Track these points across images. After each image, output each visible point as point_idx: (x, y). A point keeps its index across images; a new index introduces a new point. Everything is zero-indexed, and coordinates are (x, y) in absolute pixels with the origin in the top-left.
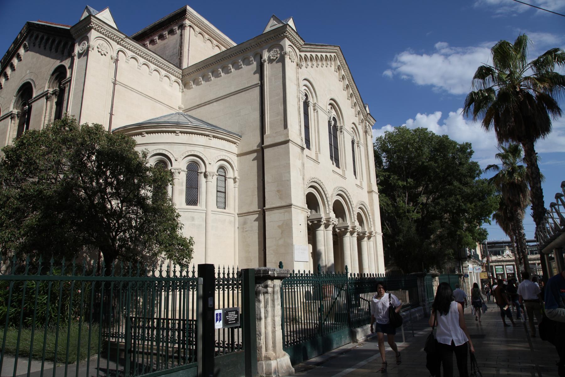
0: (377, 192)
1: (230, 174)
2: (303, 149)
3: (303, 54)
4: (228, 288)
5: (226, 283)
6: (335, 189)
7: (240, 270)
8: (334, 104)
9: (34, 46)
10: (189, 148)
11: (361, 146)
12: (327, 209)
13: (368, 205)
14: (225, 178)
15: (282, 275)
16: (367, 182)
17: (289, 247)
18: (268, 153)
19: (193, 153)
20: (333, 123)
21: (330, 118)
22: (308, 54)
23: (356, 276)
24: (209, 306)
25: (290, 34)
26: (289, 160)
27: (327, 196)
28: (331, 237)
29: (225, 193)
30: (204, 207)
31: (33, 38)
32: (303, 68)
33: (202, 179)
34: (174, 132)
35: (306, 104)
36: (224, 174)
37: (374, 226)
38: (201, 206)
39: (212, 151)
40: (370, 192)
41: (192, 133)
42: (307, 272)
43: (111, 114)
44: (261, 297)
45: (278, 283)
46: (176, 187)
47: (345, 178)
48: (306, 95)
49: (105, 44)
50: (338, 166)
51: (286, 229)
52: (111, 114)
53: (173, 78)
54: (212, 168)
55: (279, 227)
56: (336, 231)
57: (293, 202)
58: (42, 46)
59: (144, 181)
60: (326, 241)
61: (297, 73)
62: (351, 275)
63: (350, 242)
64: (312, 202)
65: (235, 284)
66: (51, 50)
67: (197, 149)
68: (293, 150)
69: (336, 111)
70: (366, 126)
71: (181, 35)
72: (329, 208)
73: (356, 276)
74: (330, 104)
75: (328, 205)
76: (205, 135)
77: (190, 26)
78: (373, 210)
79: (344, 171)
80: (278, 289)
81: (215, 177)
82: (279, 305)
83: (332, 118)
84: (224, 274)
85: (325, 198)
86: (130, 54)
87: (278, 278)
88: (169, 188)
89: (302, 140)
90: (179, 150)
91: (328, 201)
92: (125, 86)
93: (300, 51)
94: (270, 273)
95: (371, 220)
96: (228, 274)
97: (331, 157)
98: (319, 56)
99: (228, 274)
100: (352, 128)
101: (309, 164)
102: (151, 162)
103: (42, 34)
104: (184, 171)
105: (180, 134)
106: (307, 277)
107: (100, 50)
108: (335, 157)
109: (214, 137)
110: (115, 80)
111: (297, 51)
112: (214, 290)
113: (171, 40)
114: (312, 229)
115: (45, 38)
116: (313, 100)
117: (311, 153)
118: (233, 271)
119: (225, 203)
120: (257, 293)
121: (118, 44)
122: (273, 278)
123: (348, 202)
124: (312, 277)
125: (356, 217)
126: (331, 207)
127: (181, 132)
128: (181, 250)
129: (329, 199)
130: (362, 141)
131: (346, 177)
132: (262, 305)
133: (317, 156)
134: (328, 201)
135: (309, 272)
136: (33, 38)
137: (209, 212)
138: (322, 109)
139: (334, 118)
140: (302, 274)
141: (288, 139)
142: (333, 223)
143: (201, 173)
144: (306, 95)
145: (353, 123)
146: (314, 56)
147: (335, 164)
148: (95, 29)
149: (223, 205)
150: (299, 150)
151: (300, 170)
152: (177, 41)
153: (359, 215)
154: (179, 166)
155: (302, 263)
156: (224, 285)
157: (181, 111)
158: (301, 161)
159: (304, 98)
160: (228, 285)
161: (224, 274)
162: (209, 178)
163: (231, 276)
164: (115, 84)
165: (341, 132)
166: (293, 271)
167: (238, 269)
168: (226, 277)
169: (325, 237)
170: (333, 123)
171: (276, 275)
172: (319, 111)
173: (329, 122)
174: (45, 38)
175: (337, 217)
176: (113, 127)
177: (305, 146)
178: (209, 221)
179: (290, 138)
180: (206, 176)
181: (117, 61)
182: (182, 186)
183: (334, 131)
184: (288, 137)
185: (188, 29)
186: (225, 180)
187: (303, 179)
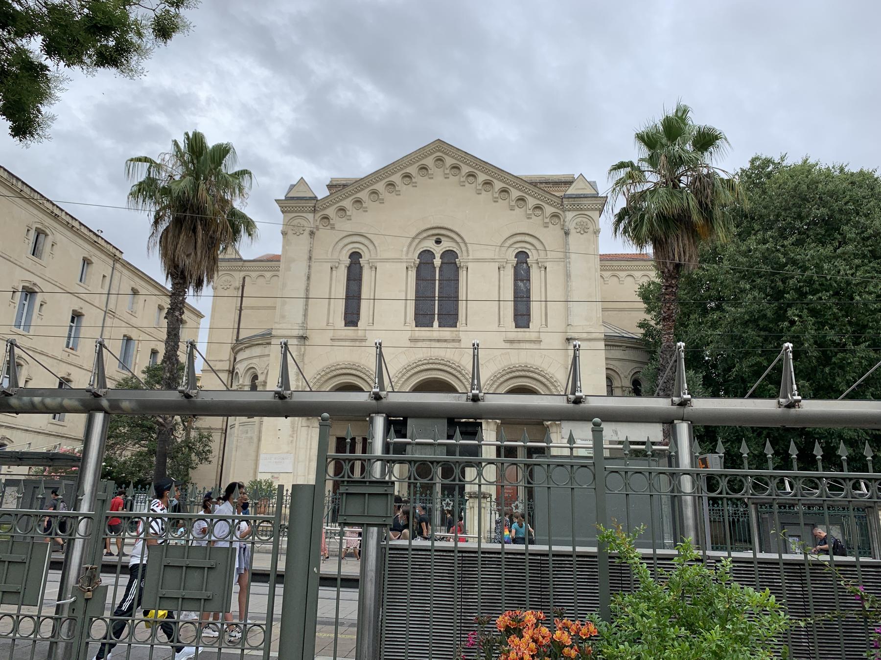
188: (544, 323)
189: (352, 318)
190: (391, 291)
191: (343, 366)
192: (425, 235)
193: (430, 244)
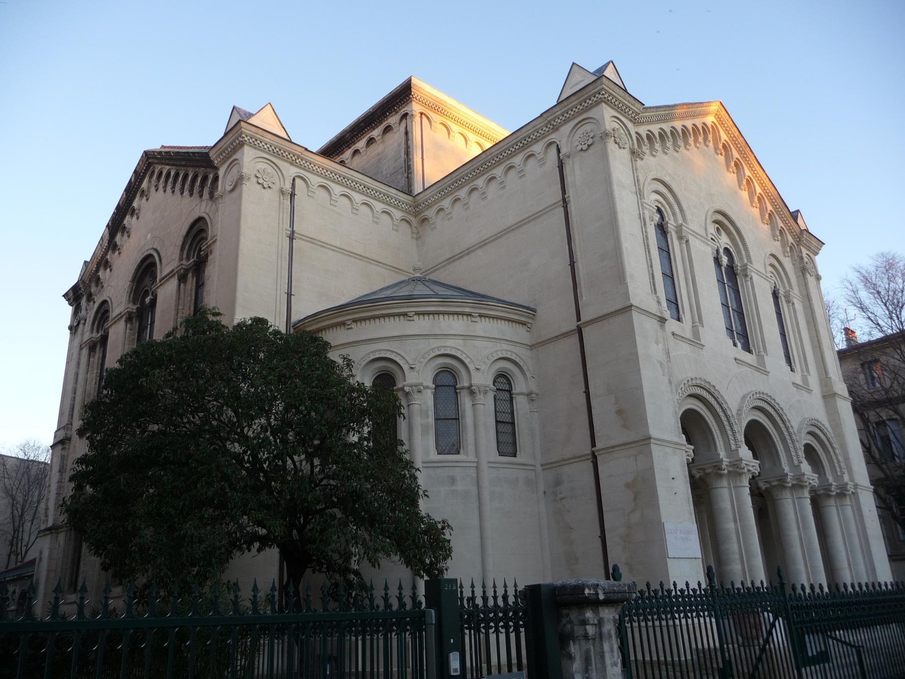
0: (846, 393)
1: (520, 386)
2: (662, 320)
3: (643, 130)
4: (487, 628)
5: (501, 615)
6: (744, 397)
7: (521, 588)
8: (724, 222)
9: (157, 190)
10: (434, 343)
11: (795, 301)
12: (732, 442)
13: (827, 425)
14: (511, 395)
15: (615, 597)
16: (819, 375)
17: (652, 531)
18: (586, 331)
19: (443, 352)
20: (725, 260)
21: (718, 251)
22: (655, 128)
23: (890, 587)
24: (452, 674)
25: (610, 94)
26: (636, 346)
27: (729, 413)
28: (748, 500)
29: (513, 423)
30: (472, 457)
31: (155, 177)
32: (646, 157)
33: (466, 401)
34: (405, 315)
35: (662, 228)
36: (507, 387)
37: (850, 471)
38: (467, 454)
39: (479, 343)
40: (829, 396)
41: (438, 313)
42: (693, 585)
43: (289, 295)
44: (574, 648)
45: (609, 615)
46: (418, 421)
47: (766, 373)
48: (659, 211)
49: (270, 169)
50: (747, 348)
51: (643, 489)
52: (289, 295)
53: (398, 214)
54: (483, 378)
55: (628, 485)
56: (759, 488)
57: (654, 432)
58: (169, 188)
59: (358, 415)
60: (739, 516)
61: (634, 169)
62: (853, 586)
63: (795, 512)
64: (692, 425)
65: (501, 619)
66: (182, 193)
67: (450, 343)
68: (643, 326)
69: (729, 234)
70: (802, 258)
71: (407, 133)
72: (735, 440)
73: (890, 587)
74: (715, 222)
75: (734, 433)
76: (463, 314)
77: (421, 114)
78: (841, 436)
79: (760, 358)
80: (609, 628)
81: (491, 395)
82: (615, 664)
83: (721, 250)
84: (495, 598)
85: (724, 418)
86: (315, 180)
87: (608, 602)
88: (402, 425)
89: (659, 302)
90: (415, 347)
91: (731, 425)
92: (311, 240)
93: (634, 121)
94: (587, 591)
95: (841, 458)
96: (505, 597)
97: (730, 330)
98: (679, 128)
99: (505, 597)
100: (772, 265)
101: (682, 350)
102: (365, 378)
103: (168, 167)
104: (427, 388)
105: (416, 317)
106: (683, 596)
107: (261, 181)
108: (741, 332)
109: (481, 316)
110: (293, 232)
111: (630, 125)
112: (463, 634)
113: (387, 146)
114: (701, 489)
115: (172, 173)
116: (676, 220)
117: (685, 328)
118: (495, 592)
119: (515, 443)
120: (565, 639)
121: (292, 164)
122: (595, 604)
123: (779, 422)
124: (705, 596)
125: (802, 454)
126: (741, 438)
127: (418, 314)
128: (425, 545)
129: (732, 420)
130: (796, 292)
131: (768, 369)
132: (577, 665)
133: (696, 334)
134: (731, 425)
135: (699, 584)
136: (155, 177)
137: (484, 466)
138: (696, 235)
139: (726, 250)
140: (655, 592)
141: (628, 304)
142: (749, 471)
143: (463, 388)
144: (659, 211)
145: (773, 255)
146: (668, 131)
147: (739, 345)
148: (250, 144)
149: (510, 449)
150: (655, 324)
151: (661, 364)
152: (399, 145)
153: (809, 449)
154: (418, 378)
155: (685, 569)
156: (496, 620)
157: (418, 275)
158: (661, 346)
159: (657, 217)
160: (487, 621)
161: (495, 598)
162: (480, 398)
163: (491, 603)
164: (291, 238)
165: (746, 276)
166: (733, 584)
167: (516, 586)
168: (500, 602)
169: (736, 504)
170: (725, 260)
171: (601, 597)
172: (692, 240)
173: (717, 261)
174: (172, 173)
175: (755, 457)
176: (295, 318)
177: (667, 314)
178: (485, 483)
179: (633, 302)
180: (472, 393)
181: (292, 195)
182: (428, 417)
183: (731, 274)
184: (629, 300)
185: (417, 119)
186: (511, 399)
187: (670, 383)
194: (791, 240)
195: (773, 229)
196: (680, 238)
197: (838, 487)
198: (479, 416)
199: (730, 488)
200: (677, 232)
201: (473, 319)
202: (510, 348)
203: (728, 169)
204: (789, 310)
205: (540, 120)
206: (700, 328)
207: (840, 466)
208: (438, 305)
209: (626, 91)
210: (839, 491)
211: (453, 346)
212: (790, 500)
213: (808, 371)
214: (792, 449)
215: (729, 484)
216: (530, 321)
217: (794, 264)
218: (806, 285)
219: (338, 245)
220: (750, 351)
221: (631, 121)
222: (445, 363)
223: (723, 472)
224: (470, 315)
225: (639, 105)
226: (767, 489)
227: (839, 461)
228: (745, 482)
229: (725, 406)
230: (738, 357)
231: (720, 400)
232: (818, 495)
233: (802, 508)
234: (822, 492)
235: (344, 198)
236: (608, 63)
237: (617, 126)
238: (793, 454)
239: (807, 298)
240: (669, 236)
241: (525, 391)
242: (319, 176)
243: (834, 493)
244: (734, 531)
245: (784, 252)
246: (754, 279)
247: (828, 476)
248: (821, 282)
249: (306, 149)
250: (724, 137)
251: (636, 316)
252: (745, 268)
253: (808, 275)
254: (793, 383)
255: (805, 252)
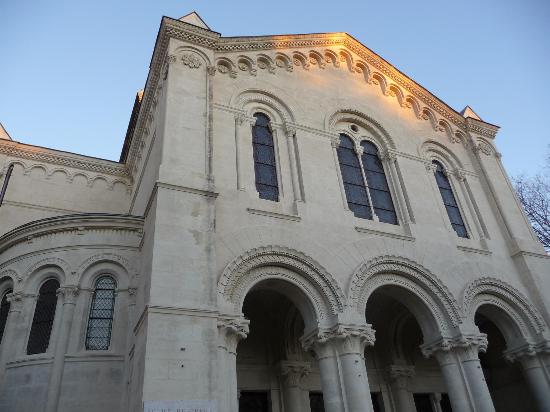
11: (468, 177)
32: (238, 76)
35: (441, 174)
36: (111, 286)
47: (413, 239)
67: (56, 255)
70: (471, 141)
95: (538, 315)
109: (87, 228)
117: (474, 242)
130: (468, 167)
133: (295, 209)
144: (434, 162)
159: (435, 167)
165: (389, 159)
188: (299, 196)
189: (268, 186)
190: (314, 171)
191: (277, 250)
192: (343, 116)
193: (346, 128)
194: (455, 128)
195: (433, 123)
196: (458, 178)
197: (536, 347)
198: (69, 315)
199: (543, 368)
200: (455, 175)
201: (80, 232)
202: (114, 251)
203: (367, 82)
204: (461, 186)
205: (152, 72)
206: (487, 241)
207: (538, 324)
208: (48, 226)
209: (209, 30)
210: (540, 350)
211: (54, 258)
212: (455, 366)
213: (487, 235)
214: (449, 311)
215: (541, 364)
216: (140, 227)
217: (466, 148)
218: (479, 162)
219: (47, 205)
220: (397, 223)
221: (209, 48)
222: (49, 273)
223: (531, 354)
224: (78, 230)
225: (215, 35)
226: (515, 361)
227: (536, 319)
228: (474, 355)
229: (322, 272)
230: (358, 226)
231: (314, 266)
232: (520, 358)
233: (469, 374)
234: (521, 354)
235: (79, 177)
236: (466, 108)
237: (481, 142)
238: (451, 315)
239: (482, 173)
240: (449, 179)
241: (126, 287)
242: (35, 160)
243: (534, 353)
244: (339, 406)
245: (451, 139)
246: (468, 180)
247: (525, 336)
248: (502, 159)
249: (19, 143)
250: (356, 58)
251: (525, 256)
252: (386, 153)
253: (482, 156)
254: (458, 247)
255: (474, 136)
